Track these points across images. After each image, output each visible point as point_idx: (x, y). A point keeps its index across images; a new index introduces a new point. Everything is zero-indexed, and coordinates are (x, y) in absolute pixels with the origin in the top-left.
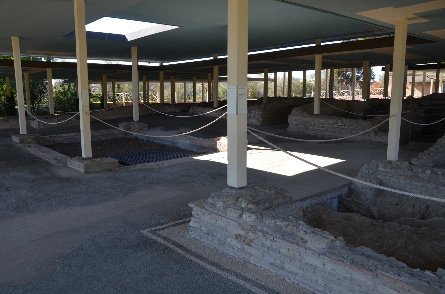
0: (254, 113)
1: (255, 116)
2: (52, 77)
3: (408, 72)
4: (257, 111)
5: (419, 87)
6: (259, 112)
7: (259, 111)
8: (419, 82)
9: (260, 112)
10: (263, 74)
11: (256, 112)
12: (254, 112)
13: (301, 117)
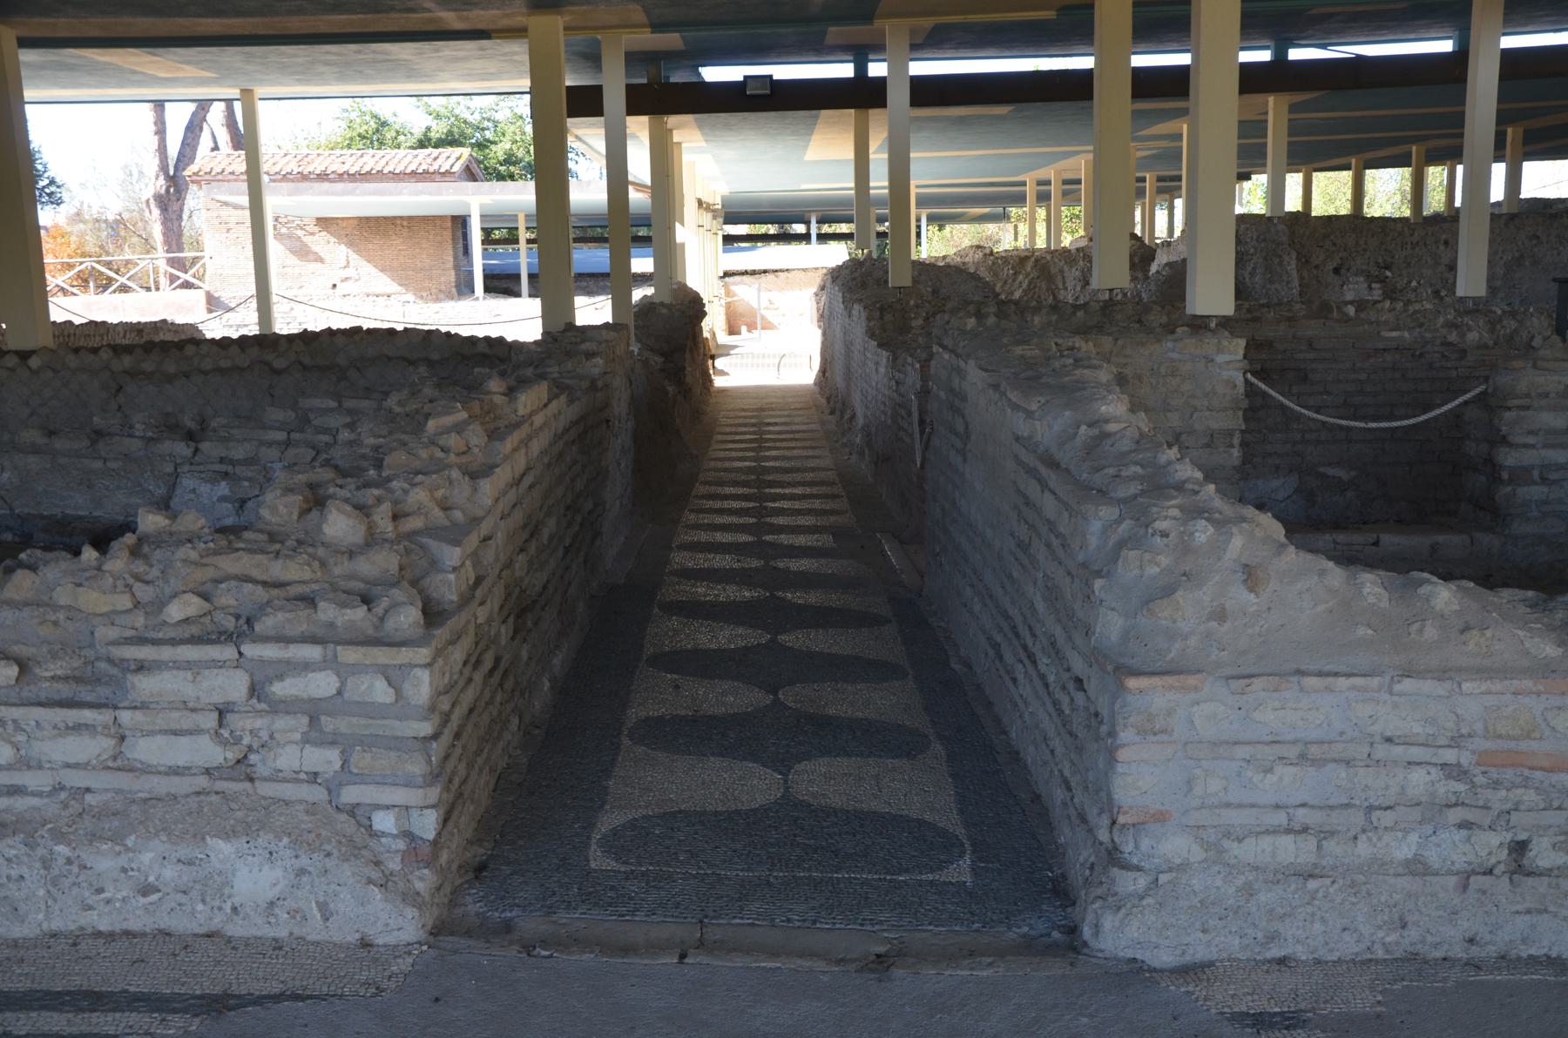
0: (222, 712)
1: (241, 768)
2: (1285, 155)
3: (872, 184)
4: (313, 652)
5: (370, 246)
6: (345, 672)
7: (349, 655)
8: (368, 219)
9: (393, 677)
10: (1522, 196)
11: (280, 689)
12: (234, 685)
13: (1441, 689)
